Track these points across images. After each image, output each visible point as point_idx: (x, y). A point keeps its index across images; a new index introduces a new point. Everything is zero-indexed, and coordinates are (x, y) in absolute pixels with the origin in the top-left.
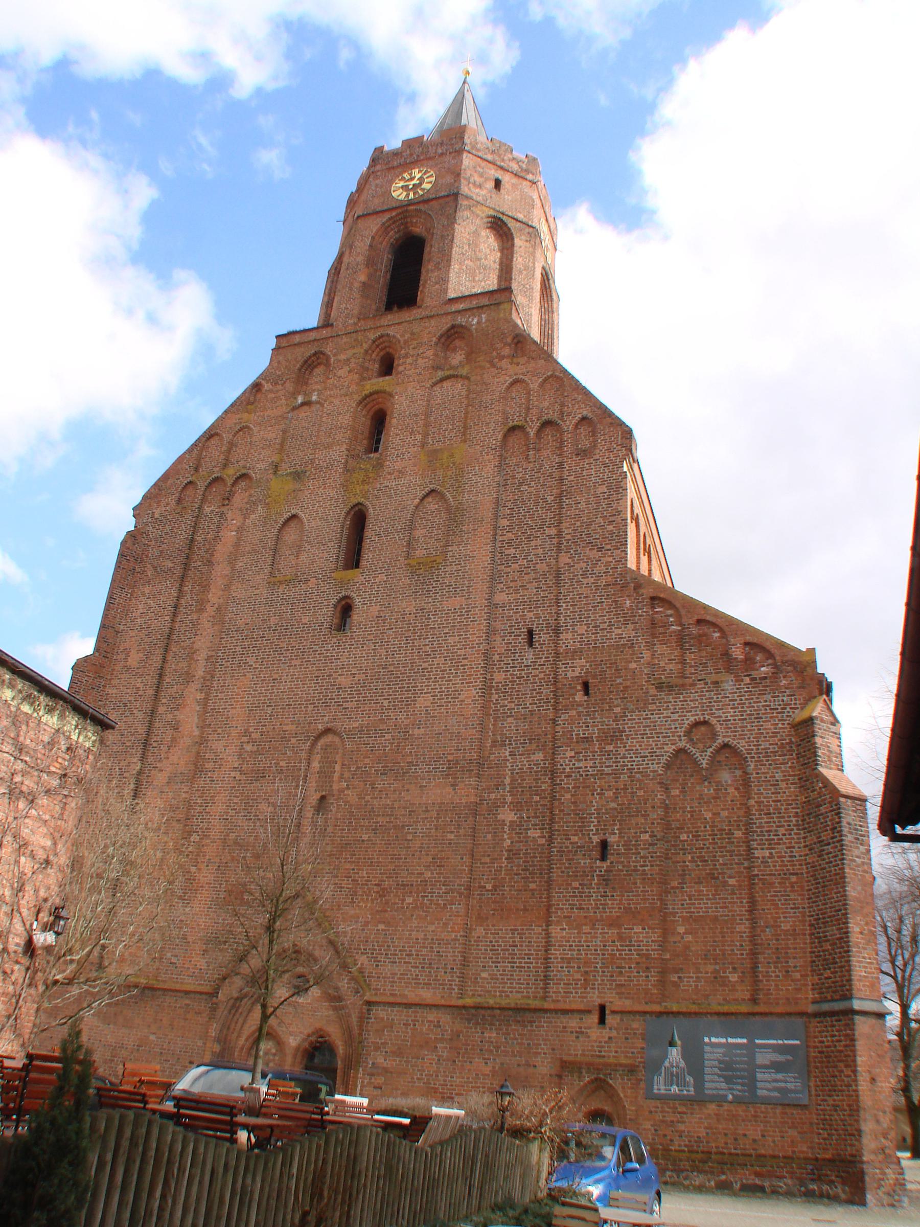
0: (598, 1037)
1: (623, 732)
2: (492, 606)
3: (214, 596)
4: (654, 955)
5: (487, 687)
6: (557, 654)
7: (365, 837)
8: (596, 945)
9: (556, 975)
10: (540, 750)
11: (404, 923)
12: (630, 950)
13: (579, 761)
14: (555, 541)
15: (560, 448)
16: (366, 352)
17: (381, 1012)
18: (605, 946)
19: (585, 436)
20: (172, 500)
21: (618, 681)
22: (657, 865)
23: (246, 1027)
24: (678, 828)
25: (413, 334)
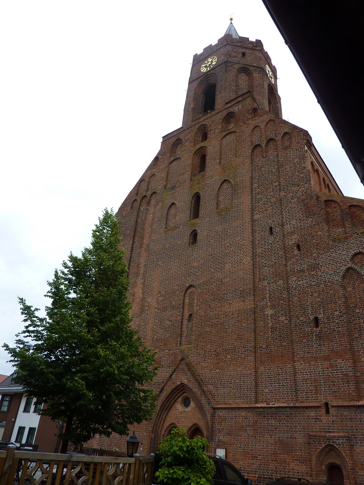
0: (327, 421)
1: (318, 264)
2: (253, 221)
3: (146, 241)
4: (351, 374)
5: (254, 256)
6: (284, 235)
7: (208, 330)
8: (319, 371)
9: (300, 388)
10: (281, 279)
11: (227, 368)
12: (337, 372)
13: (299, 281)
14: (278, 187)
15: (276, 149)
16: (196, 134)
17: (220, 413)
18: (323, 371)
19: (287, 140)
20: (129, 208)
21: (314, 241)
22: (345, 327)
23: (165, 425)
24: (354, 307)
25: (213, 121)
